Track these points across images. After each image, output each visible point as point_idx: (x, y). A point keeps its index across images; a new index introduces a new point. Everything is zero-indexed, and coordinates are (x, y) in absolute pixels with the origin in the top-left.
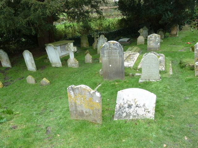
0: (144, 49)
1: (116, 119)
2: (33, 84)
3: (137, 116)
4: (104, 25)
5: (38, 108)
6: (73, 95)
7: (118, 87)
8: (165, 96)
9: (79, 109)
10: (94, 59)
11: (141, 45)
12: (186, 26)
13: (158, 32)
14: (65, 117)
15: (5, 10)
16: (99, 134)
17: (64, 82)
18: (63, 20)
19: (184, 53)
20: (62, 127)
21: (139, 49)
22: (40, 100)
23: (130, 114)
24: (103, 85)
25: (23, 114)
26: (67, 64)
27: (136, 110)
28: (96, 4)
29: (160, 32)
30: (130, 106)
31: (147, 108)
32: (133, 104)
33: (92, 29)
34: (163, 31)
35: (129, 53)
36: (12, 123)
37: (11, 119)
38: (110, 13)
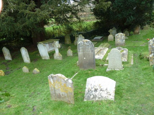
0: (113, 45)
1: (86, 100)
2: (27, 73)
3: (101, 97)
4: (83, 27)
5: (29, 91)
6: (52, 82)
7: (91, 75)
8: (125, 82)
9: (57, 92)
10: (73, 53)
11: (111, 42)
12: (147, 26)
13: (124, 31)
14: (48, 99)
15: (7, 18)
16: (71, 112)
17: (50, 71)
18: (52, 24)
19: (144, 47)
20: (44, 106)
21: (109, 45)
22: (31, 85)
23: (96, 96)
24: (79, 73)
25: (17, 96)
26: (54, 57)
27: (100, 93)
28: (75, 11)
29: (126, 32)
30: (96, 90)
31: (109, 91)
32: (99, 88)
33: (74, 30)
34: (128, 30)
35: (100, 48)
36: (8, 103)
37: (8, 100)
38: (87, 18)
